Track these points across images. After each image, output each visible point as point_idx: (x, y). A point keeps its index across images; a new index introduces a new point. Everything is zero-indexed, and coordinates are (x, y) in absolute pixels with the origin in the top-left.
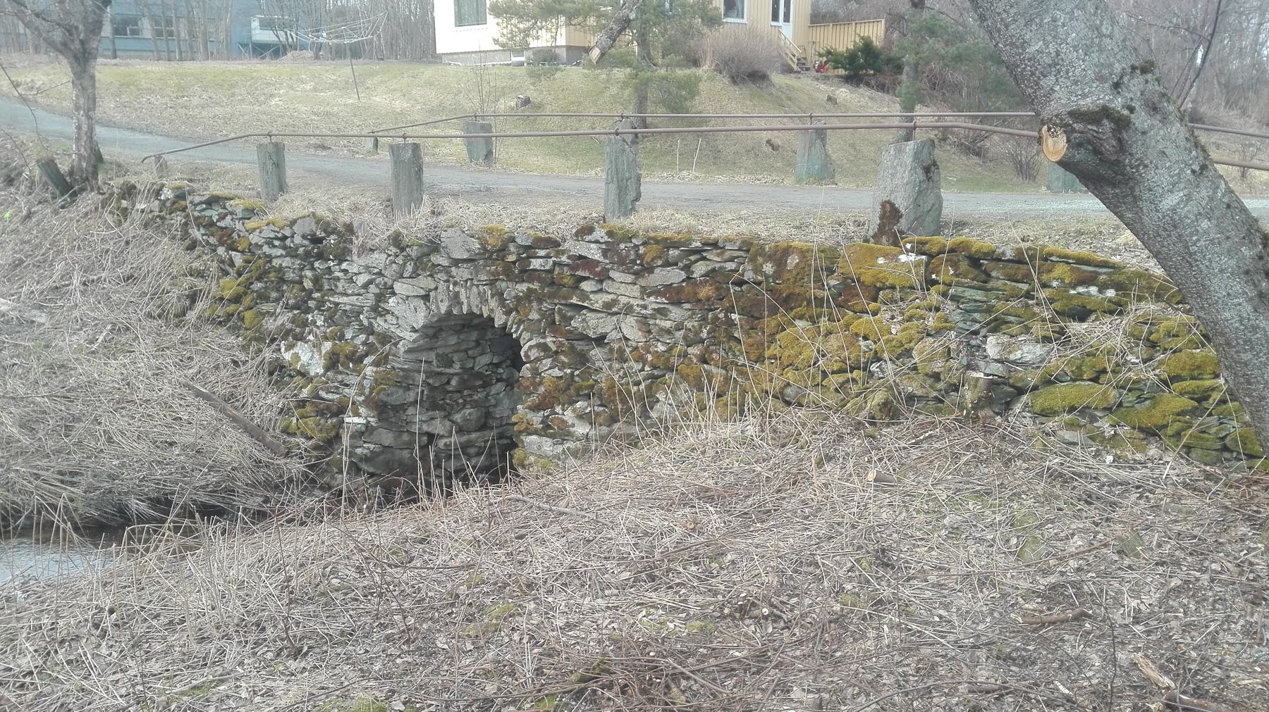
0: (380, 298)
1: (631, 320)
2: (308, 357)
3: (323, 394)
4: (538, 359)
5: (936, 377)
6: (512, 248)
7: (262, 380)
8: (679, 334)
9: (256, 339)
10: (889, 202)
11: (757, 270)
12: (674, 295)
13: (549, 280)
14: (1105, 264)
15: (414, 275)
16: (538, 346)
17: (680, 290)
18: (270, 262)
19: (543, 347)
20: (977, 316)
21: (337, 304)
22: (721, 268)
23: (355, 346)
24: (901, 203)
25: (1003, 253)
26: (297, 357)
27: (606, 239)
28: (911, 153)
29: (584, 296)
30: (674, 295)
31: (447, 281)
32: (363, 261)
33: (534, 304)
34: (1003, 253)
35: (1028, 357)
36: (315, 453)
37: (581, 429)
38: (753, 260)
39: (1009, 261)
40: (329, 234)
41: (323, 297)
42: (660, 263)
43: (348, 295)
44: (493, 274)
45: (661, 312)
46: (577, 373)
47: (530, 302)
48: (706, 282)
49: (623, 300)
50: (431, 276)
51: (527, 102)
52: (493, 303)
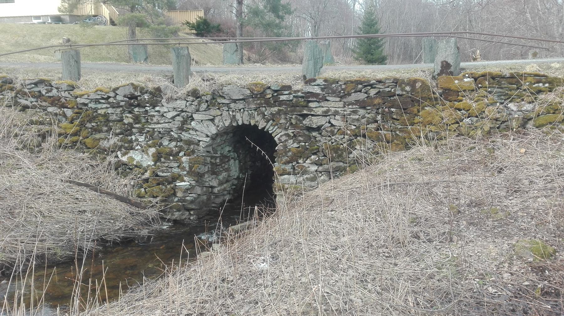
0: (184, 122)
1: (337, 117)
2: (142, 157)
3: (160, 174)
4: (286, 141)
5: (497, 120)
6: (268, 91)
7: (113, 173)
8: (363, 121)
9: (99, 153)
10: (445, 61)
11: (403, 90)
12: (363, 105)
13: (292, 105)
14: (544, 76)
15: (208, 108)
16: (285, 135)
17: (363, 101)
18: (96, 112)
19: (287, 135)
20: (502, 97)
21: (154, 129)
22: (383, 91)
23: (170, 148)
24: (450, 61)
25: (506, 75)
26: (132, 159)
27: (324, 83)
28: (454, 43)
29: (310, 109)
30: (363, 105)
31: (228, 111)
32: (171, 105)
33: (283, 116)
34: (506, 75)
35: (529, 109)
36: (163, 204)
37: (314, 168)
38: (400, 86)
39: (508, 78)
40: (143, 93)
41: (143, 126)
42: (353, 91)
43: (161, 124)
44: (259, 104)
45: (355, 112)
46: (307, 144)
47: (280, 115)
48: (377, 97)
49: (333, 109)
50: (219, 109)
51: (68, 40)
52: (258, 118)
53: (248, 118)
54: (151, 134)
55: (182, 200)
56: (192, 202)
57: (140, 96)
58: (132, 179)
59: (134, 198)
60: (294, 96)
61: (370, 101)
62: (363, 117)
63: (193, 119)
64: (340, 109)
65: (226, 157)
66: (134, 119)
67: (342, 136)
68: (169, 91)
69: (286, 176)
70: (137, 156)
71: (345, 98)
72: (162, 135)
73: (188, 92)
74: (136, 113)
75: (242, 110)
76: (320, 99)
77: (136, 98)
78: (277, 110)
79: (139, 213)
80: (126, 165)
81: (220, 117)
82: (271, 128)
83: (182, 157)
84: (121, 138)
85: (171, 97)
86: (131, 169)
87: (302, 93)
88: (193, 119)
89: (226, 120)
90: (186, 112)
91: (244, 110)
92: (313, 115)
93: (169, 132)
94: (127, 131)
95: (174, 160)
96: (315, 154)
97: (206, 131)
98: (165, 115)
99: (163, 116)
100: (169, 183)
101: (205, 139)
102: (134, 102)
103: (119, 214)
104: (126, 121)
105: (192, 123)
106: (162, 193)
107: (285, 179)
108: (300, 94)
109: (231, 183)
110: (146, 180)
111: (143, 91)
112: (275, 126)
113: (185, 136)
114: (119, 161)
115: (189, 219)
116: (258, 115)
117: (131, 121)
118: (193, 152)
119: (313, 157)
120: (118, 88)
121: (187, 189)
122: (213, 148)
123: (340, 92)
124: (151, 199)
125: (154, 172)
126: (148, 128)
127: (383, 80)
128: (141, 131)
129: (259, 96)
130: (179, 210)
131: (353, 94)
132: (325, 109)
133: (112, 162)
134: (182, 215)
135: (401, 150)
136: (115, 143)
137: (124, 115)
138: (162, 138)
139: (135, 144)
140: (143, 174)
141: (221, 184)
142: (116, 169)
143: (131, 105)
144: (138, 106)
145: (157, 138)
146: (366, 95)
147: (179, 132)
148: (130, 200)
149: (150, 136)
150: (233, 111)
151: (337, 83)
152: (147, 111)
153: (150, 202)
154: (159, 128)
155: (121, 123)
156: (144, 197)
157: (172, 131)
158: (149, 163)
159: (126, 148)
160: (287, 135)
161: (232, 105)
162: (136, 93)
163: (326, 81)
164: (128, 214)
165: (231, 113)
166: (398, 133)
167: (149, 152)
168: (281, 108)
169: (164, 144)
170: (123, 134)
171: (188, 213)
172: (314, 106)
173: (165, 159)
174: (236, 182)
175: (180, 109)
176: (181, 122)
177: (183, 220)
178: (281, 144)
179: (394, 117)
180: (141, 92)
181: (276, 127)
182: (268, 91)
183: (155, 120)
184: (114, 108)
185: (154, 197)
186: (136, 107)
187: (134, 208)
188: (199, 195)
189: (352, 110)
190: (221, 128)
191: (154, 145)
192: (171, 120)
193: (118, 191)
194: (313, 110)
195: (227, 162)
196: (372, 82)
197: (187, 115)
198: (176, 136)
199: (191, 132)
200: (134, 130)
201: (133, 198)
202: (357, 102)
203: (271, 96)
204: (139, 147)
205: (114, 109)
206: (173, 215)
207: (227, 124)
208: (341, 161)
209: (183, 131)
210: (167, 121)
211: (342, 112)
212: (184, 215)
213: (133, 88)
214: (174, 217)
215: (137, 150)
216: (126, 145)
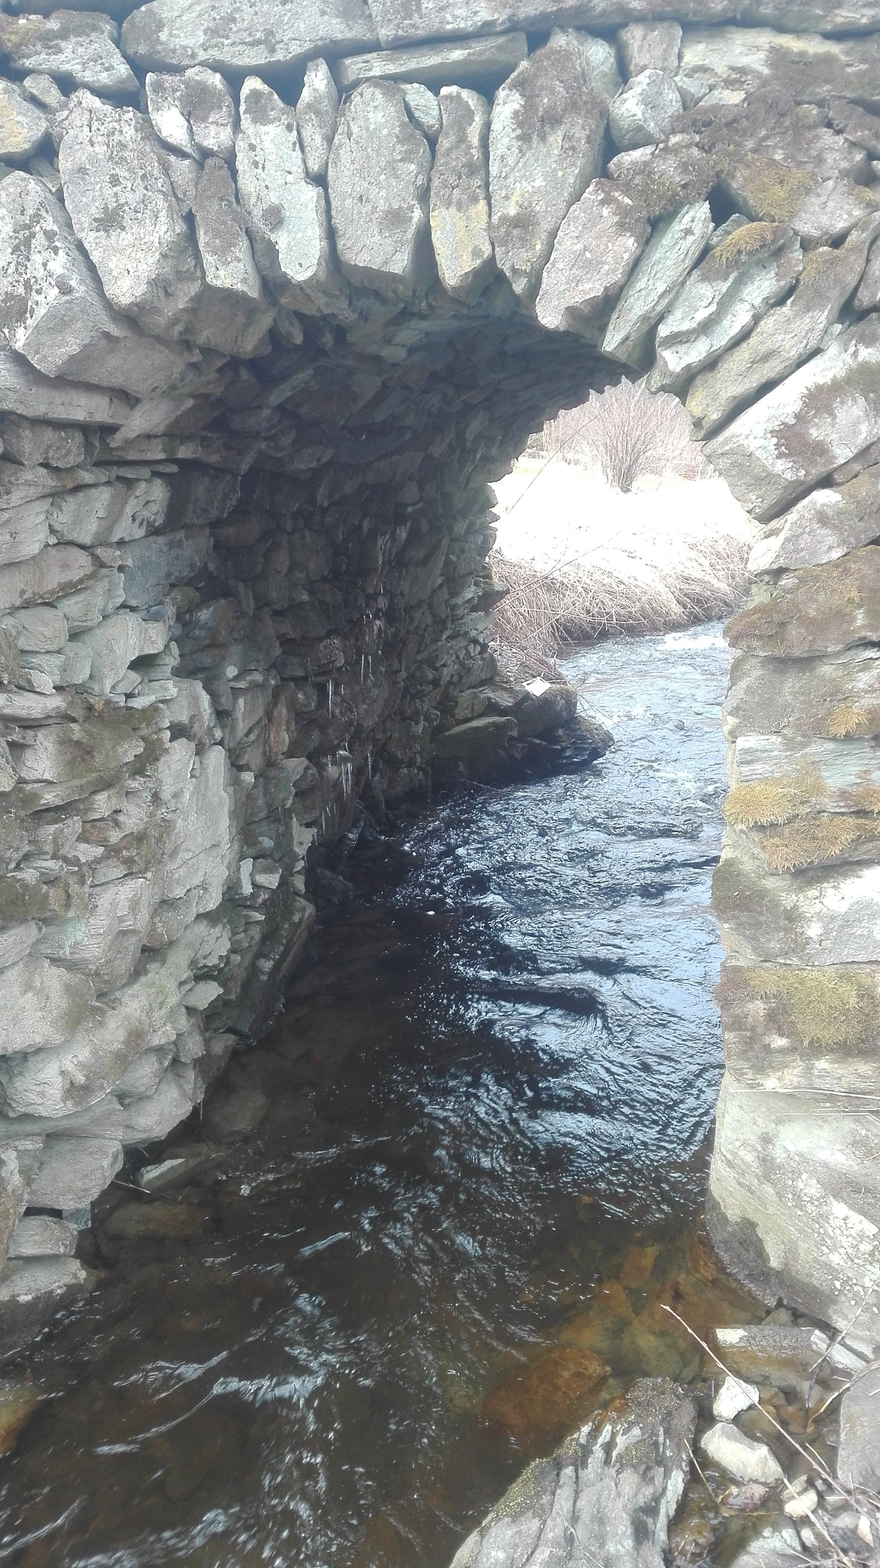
47: (799, 134)
53: (394, 191)
65: (124, 719)
75: (317, 80)
78: (757, 61)
82: (704, 296)
89: (109, 221)
91: (343, 91)
109: (179, 962)
112: (743, 267)
116: (533, 126)
141: (92, 997)
150: (196, 106)
165: (171, 123)
168: (814, 47)
174: (216, 944)
178: (823, 497)
181: (762, 286)
190: (58, 322)
195: (139, 768)
207: (131, 268)
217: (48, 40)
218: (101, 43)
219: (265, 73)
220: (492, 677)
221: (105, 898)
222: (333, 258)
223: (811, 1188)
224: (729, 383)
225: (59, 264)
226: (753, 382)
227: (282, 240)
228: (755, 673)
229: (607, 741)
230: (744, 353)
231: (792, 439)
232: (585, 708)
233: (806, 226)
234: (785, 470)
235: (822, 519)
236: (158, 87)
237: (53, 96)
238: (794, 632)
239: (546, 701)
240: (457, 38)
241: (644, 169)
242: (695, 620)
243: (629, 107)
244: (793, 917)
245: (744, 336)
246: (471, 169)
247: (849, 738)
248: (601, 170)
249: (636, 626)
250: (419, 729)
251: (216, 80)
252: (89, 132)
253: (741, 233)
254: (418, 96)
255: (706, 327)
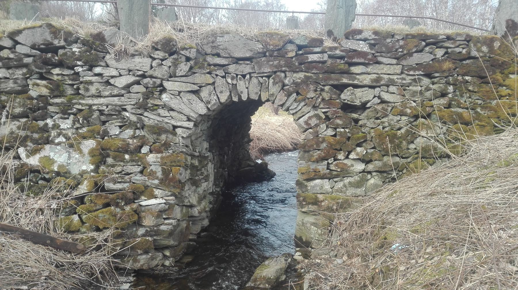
0: (148, 95)
1: (392, 89)
2: (69, 158)
4: (317, 125)
8: (428, 94)
10: (510, 20)
11: (479, 50)
15: (191, 71)
19: (317, 116)
21: (90, 106)
22: (452, 51)
23: (124, 140)
26: (50, 161)
27: (373, 36)
32: (124, 64)
33: (312, 87)
36: (119, 241)
37: (360, 167)
41: (70, 100)
42: (414, 50)
44: (276, 66)
47: (307, 85)
48: (446, 60)
53: (257, 90)
54: (86, 116)
55: (153, 232)
56: (171, 234)
57: (63, 47)
58: (53, 198)
59: (60, 235)
60: (330, 57)
61: (437, 64)
62: (428, 89)
63: (164, 90)
64: (395, 77)
66: (50, 89)
67: (398, 118)
68: (120, 42)
69: (318, 181)
70: (58, 156)
71: (405, 59)
72: (105, 117)
73: (157, 43)
74: (55, 78)
75: (248, 76)
76: (370, 60)
77: (55, 50)
78: (302, 76)
79: (74, 264)
80: (38, 172)
81: (212, 88)
82: (295, 105)
83: (147, 154)
84: (25, 123)
85: (125, 51)
86: (48, 180)
87: (342, 51)
88: (164, 90)
90: (151, 77)
92: (356, 86)
93: (120, 112)
94: (37, 111)
95: (132, 161)
96: (359, 145)
97: (187, 111)
98: (112, 81)
99: (108, 83)
100: (129, 202)
101: (186, 124)
102: (53, 57)
103: (35, 270)
104: (33, 93)
105: (164, 96)
106: (115, 221)
107: (316, 185)
108: (338, 52)
110: (81, 200)
111: (70, 39)
112: (300, 101)
113: (151, 118)
114: (24, 165)
115: (163, 265)
116: (274, 83)
117: (45, 91)
118: (167, 145)
119: (359, 149)
120: (19, 32)
121: (161, 212)
122: (192, 142)
123: (397, 50)
124: (95, 234)
125: (96, 184)
126: (80, 104)
127: (454, 37)
128: (65, 113)
129: (275, 54)
130: (146, 252)
131: (415, 55)
132: (374, 76)
133: (9, 169)
134: (152, 258)
135: (488, 134)
136: (12, 133)
137: (29, 82)
138: (104, 123)
139: (53, 133)
140: (75, 187)
142: (17, 180)
143: (47, 63)
144: (60, 64)
145: (97, 122)
146: (432, 57)
147: (140, 111)
148: (52, 239)
149: (85, 118)
150: (233, 78)
151: (393, 36)
152: (77, 74)
153: (93, 239)
154: (101, 105)
155: (25, 96)
156: (78, 231)
157: (125, 110)
158: (84, 168)
159: (36, 142)
160: (317, 116)
161: (232, 68)
162: (56, 42)
163: (376, 33)
164: (53, 268)
165: (229, 81)
166: (479, 110)
167: (82, 147)
168: (309, 74)
169: (112, 133)
170: (27, 117)
171: (160, 255)
172: (359, 71)
173: (114, 158)
175: (140, 73)
176: (143, 94)
177: (152, 269)
178: (310, 130)
179: (471, 88)
180: (65, 40)
181: (303, 104)
182: (290, 47)
183: (93, 90)
184: (8, 68)
185: (98, 230)
186: (55, 66)
187: (61, 253)
188: (179, 220)
189: (413, 78)
190: (214, 104)
191: (91, 135)
192: (123, 92)
193: (24, 223)
194: (356, 79)
196: (441, 37)
197: (154, 83)
198: (134, 118)
199: (161, 111)
200: (51, 109)
201: (59, 235)
202: (419, 66)
203: (294, 54)
204: (61, 139)
205: (10, 71)
206: (135, 261)
207: (224, 98)
208: (397, 155)
209: (146, 110)
210: (116, 92)
211: (400, 81)
212: (156, 258)
213: (51, 33)
214: (137, 266)
215: (59, 144)
216: (36, 136)
217: (215, 70)
218: (222, 71)
219: (241, 75)
220: (249, 158)
221: (203, 184)
222: (248, 98)
223: (308, 225)
224: (298, 115)
225: (215, 97)
226: (301, 115)
227: (242, 95)
228: (302, 153)
229: (274, 174)
230: (300, 112)
231: (306, 123)
232: (269, 167)
233: (308, 96)
234: (306, 127)
235: (310, 133)
236: (228, 76)
237: (215, 77)
238: (306, 147)
239: (261, 164)
240: (266, 73)
241: (288, 89)
242: (295, 149)
243: (286, 81)
244: (306, 186)
245: (300, 109)
246: (267, 88)
247: (313, 162)
248: (282, 89)
249: (280, 150)
250: (235, 169)
251: (235, 75)
252: (219, 81)
253: (300, 97)
254: (260, 79)
255: (295, 108)
